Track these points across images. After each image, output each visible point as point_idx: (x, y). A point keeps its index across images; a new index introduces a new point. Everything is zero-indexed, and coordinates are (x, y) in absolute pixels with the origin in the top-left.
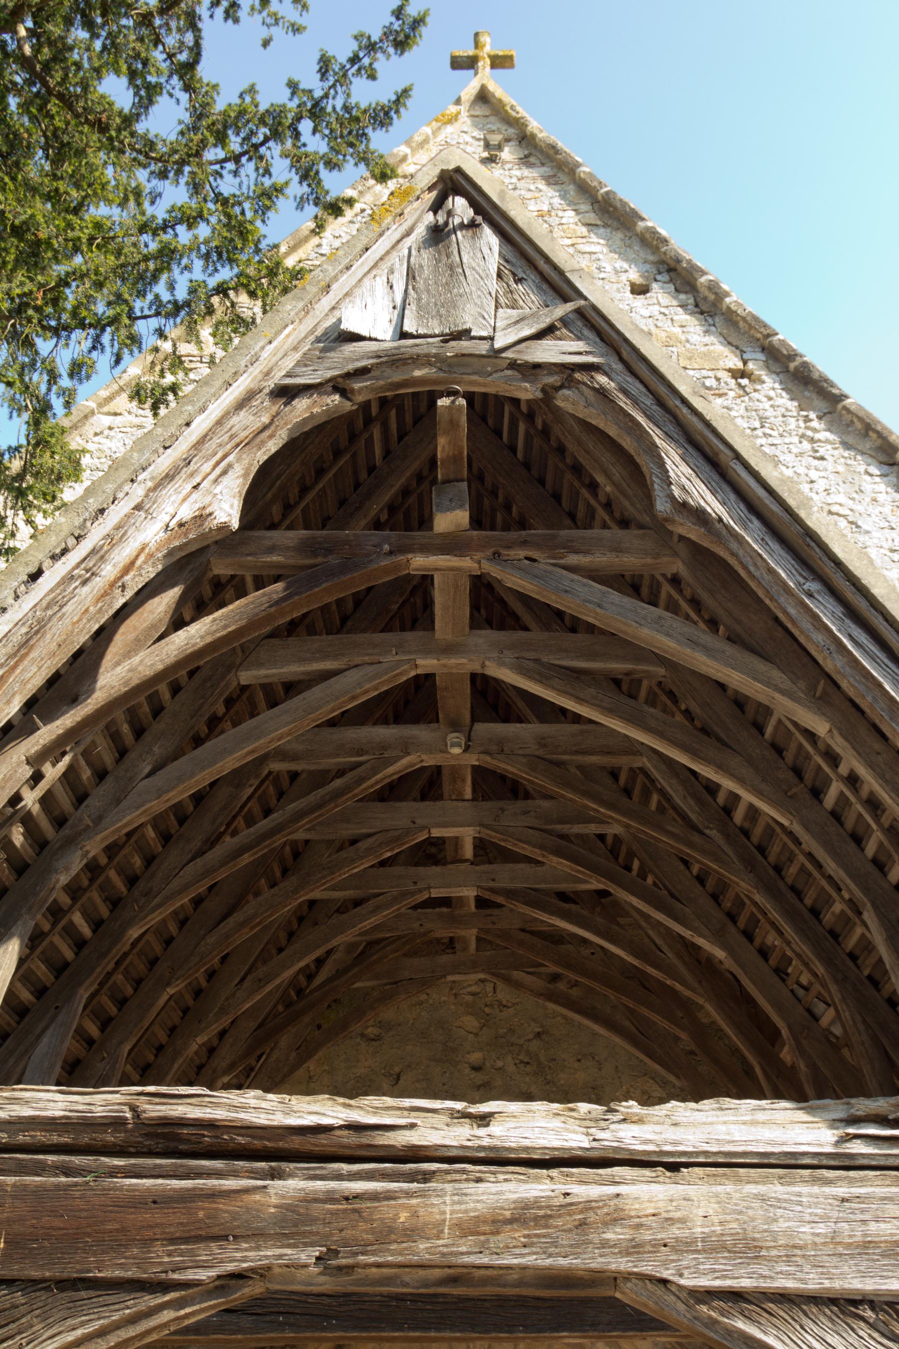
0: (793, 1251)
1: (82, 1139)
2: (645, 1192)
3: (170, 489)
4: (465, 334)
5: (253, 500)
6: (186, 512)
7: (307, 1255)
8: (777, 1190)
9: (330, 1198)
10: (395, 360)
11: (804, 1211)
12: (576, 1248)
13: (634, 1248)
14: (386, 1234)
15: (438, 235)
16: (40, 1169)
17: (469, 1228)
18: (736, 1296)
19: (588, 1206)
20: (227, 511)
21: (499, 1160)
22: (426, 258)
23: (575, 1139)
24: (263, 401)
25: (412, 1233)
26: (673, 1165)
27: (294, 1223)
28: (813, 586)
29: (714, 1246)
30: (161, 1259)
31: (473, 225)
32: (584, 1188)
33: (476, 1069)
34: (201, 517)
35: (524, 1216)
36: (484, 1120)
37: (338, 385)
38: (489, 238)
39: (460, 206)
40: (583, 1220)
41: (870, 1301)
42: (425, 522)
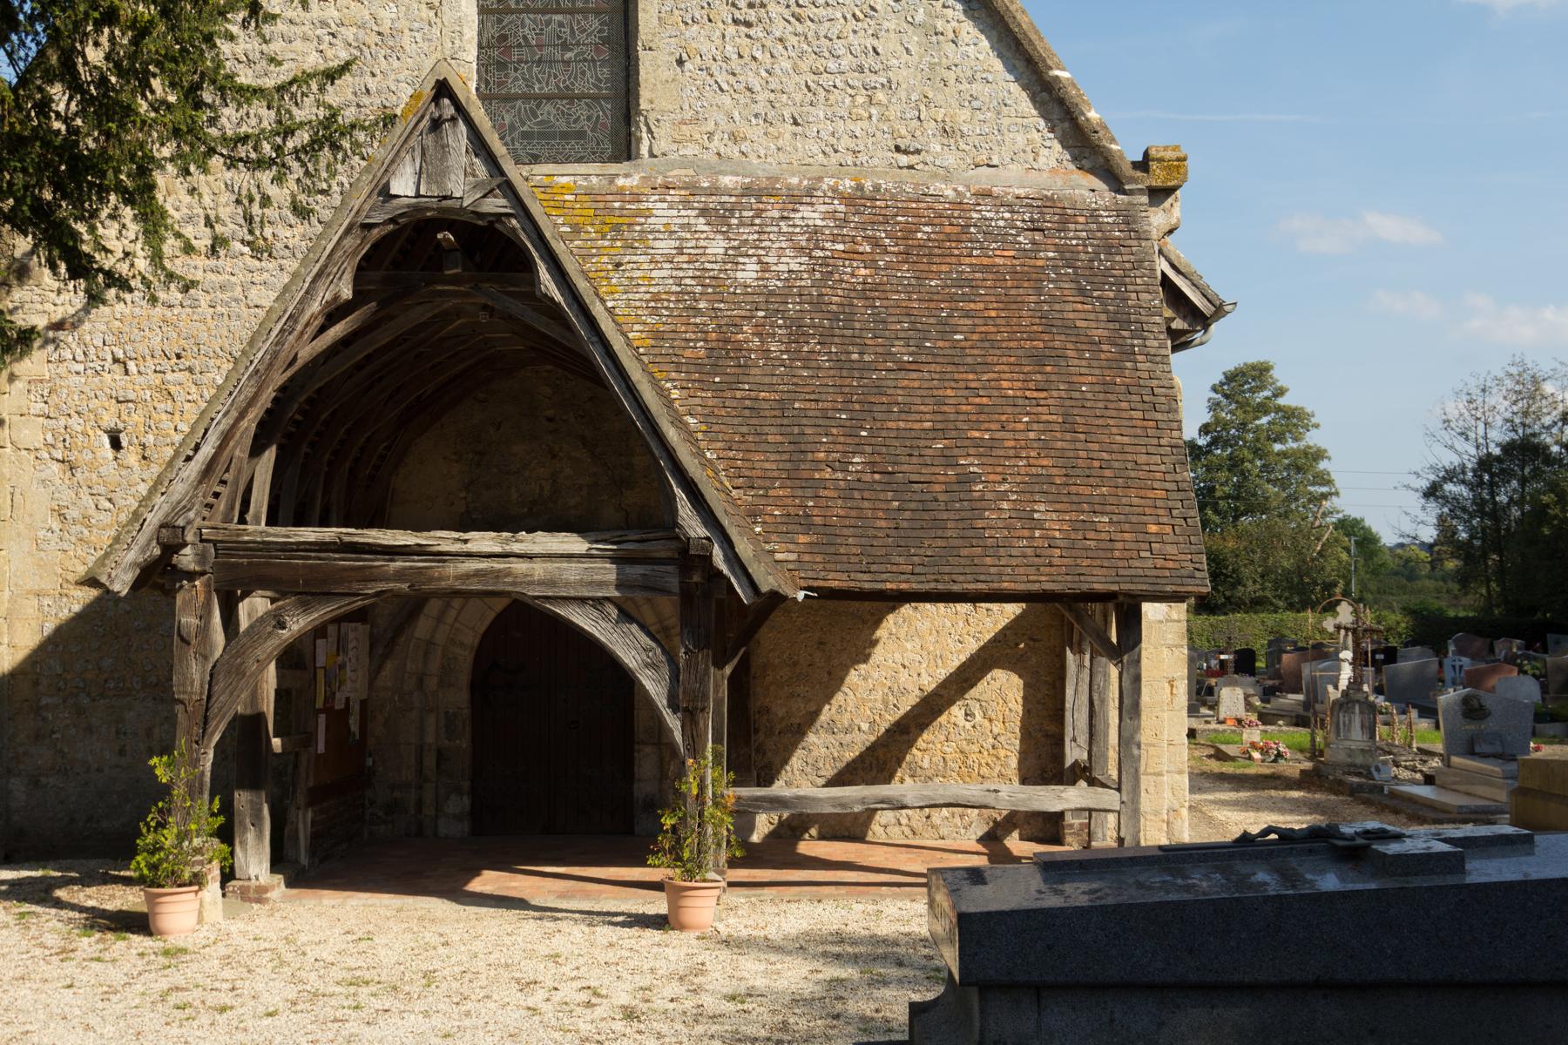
0: (567, 584)
1: (322, 547)
2: (520, 566)
3: (320, 283)
4: (451, 198)
5: (357, 281)
6: (328, 296)
7: (405, 586)
8: (565, 565)
9: (411, 568)
10: (417, 209)
11: (572, 572)
12: (495, 584)
13: (514, 584)
14: (431, 579)
15: (436, 125)
16: (310, 558)
17: (457, 578)
18: (547, 598)
19: (499, 571)
20: (347, 293)
21: (470, 555)
22: (429, 140)
23: (497, 549)
24: (356, 231)
25: (440, 579)
26: (530, 557)
27: (400, 575)
28: (595, 339)
29: (541, 583)
30: (355, 587)
31: (453, 119)
32: (497, 565)
33: (550, 420)
34: (336, 297)
35: (478, 574)
36: (466, 541)
37: (392, 220)
38: (462, 127)
39: (448, 110)
40: (497, 575)
41: (592, 599)
42: (440, 268)
